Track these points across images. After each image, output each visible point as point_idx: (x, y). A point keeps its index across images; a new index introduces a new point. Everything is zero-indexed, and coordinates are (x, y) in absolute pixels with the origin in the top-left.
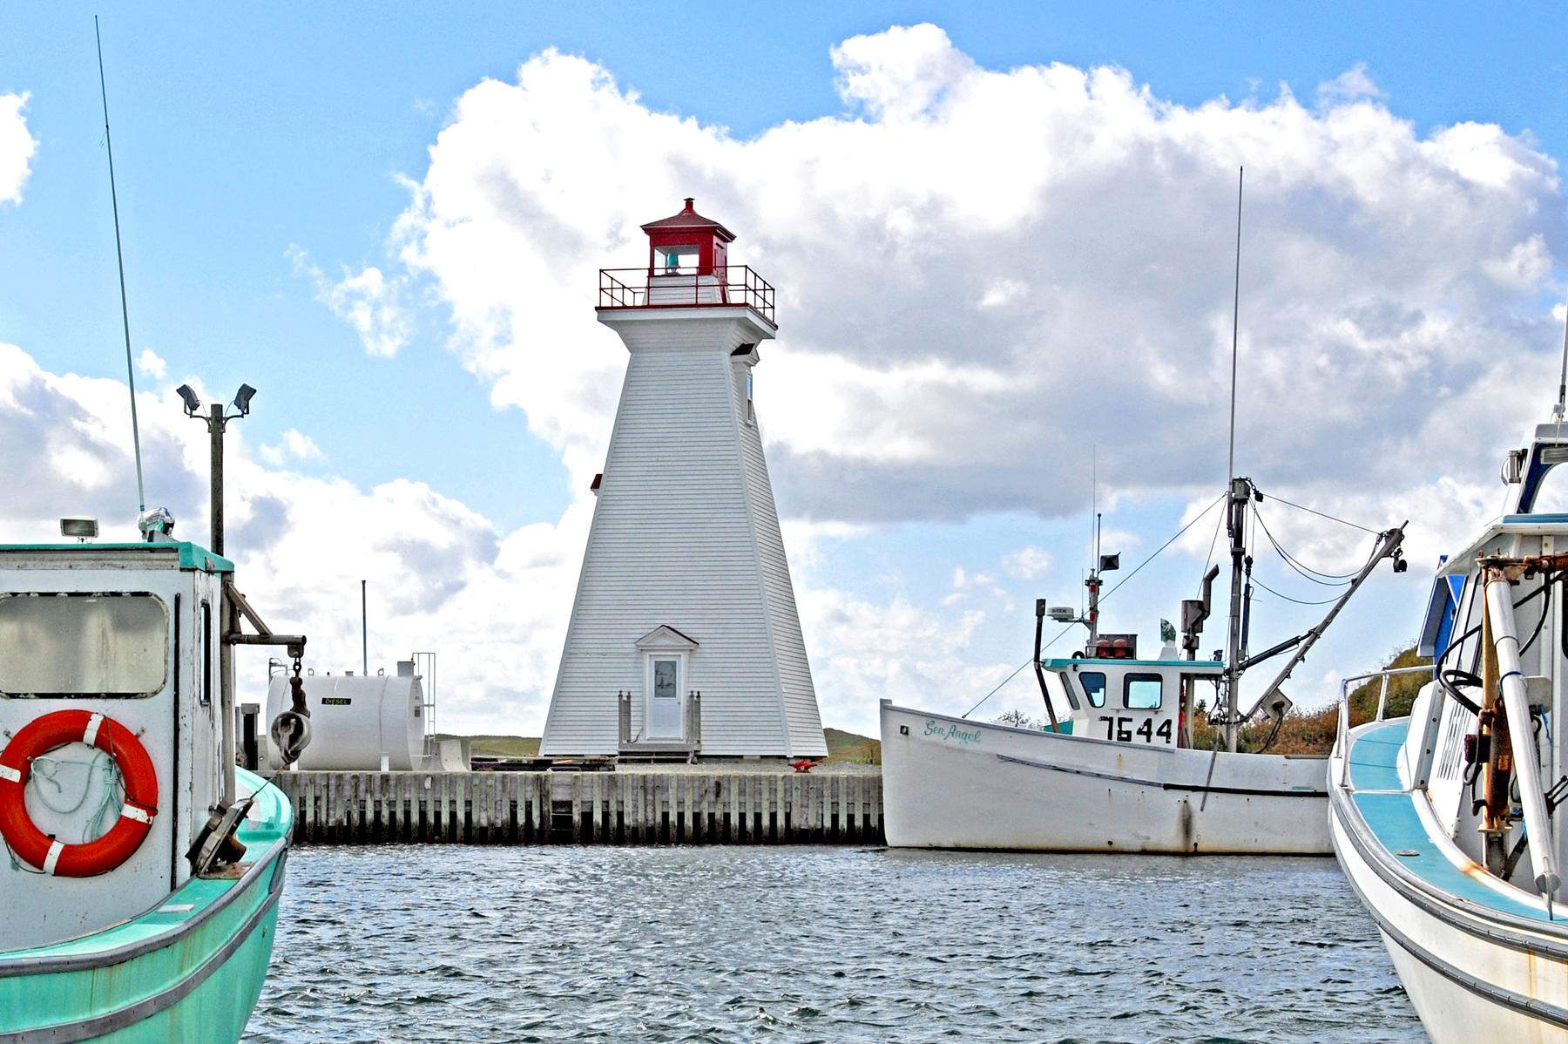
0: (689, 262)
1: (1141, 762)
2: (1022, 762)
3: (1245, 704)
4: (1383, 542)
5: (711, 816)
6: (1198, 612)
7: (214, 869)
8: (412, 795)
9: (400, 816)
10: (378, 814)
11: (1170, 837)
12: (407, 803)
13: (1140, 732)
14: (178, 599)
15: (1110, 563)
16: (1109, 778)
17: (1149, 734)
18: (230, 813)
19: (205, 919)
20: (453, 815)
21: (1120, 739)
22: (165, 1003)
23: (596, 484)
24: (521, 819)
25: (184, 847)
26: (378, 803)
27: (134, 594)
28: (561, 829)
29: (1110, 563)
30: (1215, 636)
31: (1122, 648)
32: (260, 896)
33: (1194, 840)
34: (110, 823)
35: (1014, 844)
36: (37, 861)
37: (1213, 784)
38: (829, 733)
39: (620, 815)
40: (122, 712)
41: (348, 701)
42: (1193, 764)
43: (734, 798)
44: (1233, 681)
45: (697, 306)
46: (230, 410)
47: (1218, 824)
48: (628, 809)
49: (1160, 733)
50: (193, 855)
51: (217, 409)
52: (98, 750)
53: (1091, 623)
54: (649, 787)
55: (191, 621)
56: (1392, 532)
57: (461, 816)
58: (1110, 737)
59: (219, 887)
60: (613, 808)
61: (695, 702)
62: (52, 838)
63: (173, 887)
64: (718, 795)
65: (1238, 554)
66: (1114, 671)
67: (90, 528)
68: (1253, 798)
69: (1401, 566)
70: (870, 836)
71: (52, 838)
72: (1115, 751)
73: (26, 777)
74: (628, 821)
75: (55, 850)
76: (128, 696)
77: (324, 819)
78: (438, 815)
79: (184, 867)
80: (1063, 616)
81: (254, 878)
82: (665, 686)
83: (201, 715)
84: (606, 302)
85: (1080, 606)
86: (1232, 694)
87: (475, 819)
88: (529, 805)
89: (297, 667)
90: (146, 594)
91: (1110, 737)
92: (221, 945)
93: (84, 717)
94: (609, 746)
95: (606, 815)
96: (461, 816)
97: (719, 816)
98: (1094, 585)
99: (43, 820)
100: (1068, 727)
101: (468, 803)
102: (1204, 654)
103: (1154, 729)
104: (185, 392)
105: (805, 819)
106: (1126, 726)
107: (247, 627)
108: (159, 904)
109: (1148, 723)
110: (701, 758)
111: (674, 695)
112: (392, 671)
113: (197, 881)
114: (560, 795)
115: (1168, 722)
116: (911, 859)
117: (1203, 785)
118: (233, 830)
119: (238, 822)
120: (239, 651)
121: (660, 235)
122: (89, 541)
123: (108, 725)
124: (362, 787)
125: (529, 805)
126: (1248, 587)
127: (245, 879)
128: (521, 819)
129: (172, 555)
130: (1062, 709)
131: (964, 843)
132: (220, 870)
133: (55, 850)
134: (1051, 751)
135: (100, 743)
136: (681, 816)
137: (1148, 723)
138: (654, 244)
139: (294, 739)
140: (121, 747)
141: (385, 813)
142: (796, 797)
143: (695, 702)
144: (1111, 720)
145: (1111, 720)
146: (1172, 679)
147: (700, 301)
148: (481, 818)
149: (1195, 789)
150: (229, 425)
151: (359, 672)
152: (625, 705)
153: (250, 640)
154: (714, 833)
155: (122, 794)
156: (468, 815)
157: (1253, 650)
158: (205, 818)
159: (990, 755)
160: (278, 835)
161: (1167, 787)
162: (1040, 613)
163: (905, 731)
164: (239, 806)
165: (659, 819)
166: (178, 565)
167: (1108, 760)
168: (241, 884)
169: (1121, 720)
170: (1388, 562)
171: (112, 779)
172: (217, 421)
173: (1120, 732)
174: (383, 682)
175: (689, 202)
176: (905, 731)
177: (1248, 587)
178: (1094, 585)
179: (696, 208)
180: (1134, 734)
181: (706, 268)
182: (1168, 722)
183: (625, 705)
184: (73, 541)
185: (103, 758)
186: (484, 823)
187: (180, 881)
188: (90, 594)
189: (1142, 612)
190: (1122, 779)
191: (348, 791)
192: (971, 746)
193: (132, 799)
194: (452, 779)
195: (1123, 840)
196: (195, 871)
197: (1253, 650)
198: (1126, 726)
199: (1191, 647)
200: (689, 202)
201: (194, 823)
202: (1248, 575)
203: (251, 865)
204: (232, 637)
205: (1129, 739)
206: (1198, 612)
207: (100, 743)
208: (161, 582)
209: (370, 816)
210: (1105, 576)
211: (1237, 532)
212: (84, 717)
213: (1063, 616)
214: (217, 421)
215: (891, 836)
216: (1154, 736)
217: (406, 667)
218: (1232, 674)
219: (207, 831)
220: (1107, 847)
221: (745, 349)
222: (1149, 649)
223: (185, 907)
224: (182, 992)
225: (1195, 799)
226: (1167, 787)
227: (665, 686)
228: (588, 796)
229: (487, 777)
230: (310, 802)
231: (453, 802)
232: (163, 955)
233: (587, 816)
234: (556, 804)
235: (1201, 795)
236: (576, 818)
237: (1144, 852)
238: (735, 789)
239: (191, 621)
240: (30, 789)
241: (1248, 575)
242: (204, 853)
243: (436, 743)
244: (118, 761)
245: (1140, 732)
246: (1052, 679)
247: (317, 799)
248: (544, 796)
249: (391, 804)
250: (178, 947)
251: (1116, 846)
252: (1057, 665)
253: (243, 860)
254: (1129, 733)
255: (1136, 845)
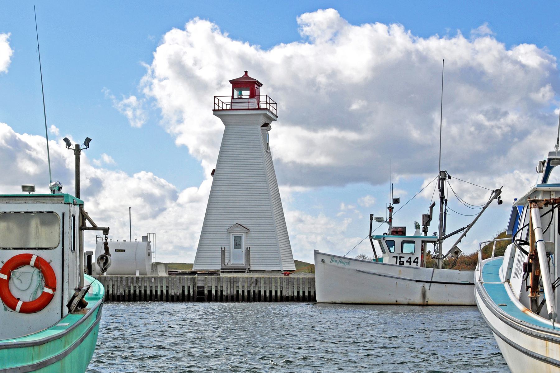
0: (246, 94)
1: (407, 272)
2: (365, 272)
3: (445, 252)
4: (494, 194)
5: (254, 291)
6: (428, 219)
7: (76, 310)
8: (147, 284)
9: (143, 292)
10: (135, 291)
11: (418, 299)
12: (145, 287)
13: (407, 262)
14: (63, 214)
15: (396, 201)
16: (396, 278)
17: (410, 262)
18: (82, 291)
19: (73, 328)
20: (162, 291)
21: (400, 264)
22: (59, 358)
23: (213, 173)
24: (186, 293)
25: (66, 303)
26: (135, 287)
27: (48, 212)
28: (201, 296)
29: (396, 201)
30: (434, 227)
31: (400, 232)
32: (93, 320)
33: (426, 300)
34: (39, 294)
35: (362, 301)
36: (14, 308)
37: (433, 280)
38: (296, 262)
39: (222, 291)
40: (44, 255)
41: (124, 251)
42: (426, 273)
43: (262, 285)
44: (440, 244)
45: (249, 109)
46: (82, 146)
47: (435, 294)
48: (224, 289)
49: (414, 262)
50: (69, 306)
51: (77, 146)
52: (35, 268)
53: (390, 223)
54: (232, 281)
55: (68, 222)
56: (497, 190)
57: (165, 292)
58: (396, 263)
59: (78, 317)
60: (219, 289)
61: (248, 251)
62: (19, 299)
63: (62, 317)
64: (256, 284)
65: (442, 198)
66: (398, 240)
67: (32, 189)
68: (447, 285)
69: (500, 202)
70: (311, 299)
71: (19, 299)
72: (398, 268)
73: (9, 278)
74: (224, 293)
75: (20, 304)
76: (46, 249)
77: (116, 293)
78: (156, 291)
79: (66, 310)
80: (380, 220)
81: (91, 314)
82: (237, 245)
83: (72, 255)
84: (217, 108)
85: (386, 217)
86: (440, 248)
87: (169, 292)
88: (189, 288)
89: (106, 238)
90: (52, 212)
91: (396, 263)
92: (79, 338)
93: (30, 256)
94: (217, 267)
95: (216, 291)
96: (165, 292)
97: (257, 291)
98: (391, 209)
99: (15, 293)
100: (381, 260)
101: (167, 287)
102: (430, 234)
103: (412, 260)
104: (66, 140)
105: (287, 293)
106: (402, 260)
107: (88, 224)
108: (57, 323)
109: (410, 258)
110: (250, 271)
111: (241, 248)
112: (140, 240)
113: (70, 315)
114: (200, 284)
115: (417, 258)
116: (325, 307)
117: (430, 280)
118: (83, 296)
119: (85, 294)
120: (85, 232)
121: (236, 84)
122: (32, 193)
123: (38, 259)
124: (129, 281)
125: (189, 288)
126: (446, 210)
127: (88, 314)
128: (186, 293)
129: (62, 198)
130: (379, 253)
131: (344, 301)
132: (78, 311)
133: (20, 304)
134: (375, 269)
135: (36, 265)
136: (243, 292)
137: (410, 258)
138: (234, 88)
139: (105, 264)
140: (43, 267)
141: (138, 290)
142: (284, 285)
143: (248, 251)
144: (397, 257)
145: (397, 257)
146: (419, 242)
147: (250, 108)
148: (172, 292)
149: (427, 282)
150: (82, 152)
151: (128, 240)
152: (223, 252)
153: (89, 229)
154: (255, 298)
155: (44, 284)
156: (167, 291)
157: (447, 232)
158: (73, 292)
159: (354, 270)
160: (99, 299)
161: (417, 281)
162: (372, 219)
163: (323, 261)
164: (85, 288)
165: (235, 292)
166: (63, 202)
167: (395, 272)
168: (86, 316)
169: (400, 257)
170: (496, 201)
171: (40, 278)
172: (77, 151)
173: (400, 262)
174: (137, 243)
175: (246, 72)
176: (323, 261)
177: (446, 210)
178: (391, 209)
179: (249, 74)
180: (405, 262)
181: (252, 96)
182: (417, 258)
183: (223, 252)
184: (26, 193)
185: (36, 271)
186: (173, 294)
187: (64, 315)
188: (32, 212)
189: (408, 219)
190: (401, 278)
191: (124, 283)
192: (347, 267)
193: (47, 286)
194: (161, 278)
195: (401, 300)
196: (70, 311)
197: (447, 232)
198: (402, 260)
199: (425, 231)
200: (246, 72)
201: (69, 294)
202: (446, 205)
203: (90, 309)
204: (83, 227)
205: (403, 264)
206: (428, 219)
207: (36, 265)
208: (58, 208)
209: (132, 291)
210: (395, 206)
211: (442, 190)
212: (30, 256)
213: (380, 220)
214: (77, 151)
215: (318, 299)
216: (412, 263)
217: (145, 238)
218: (440, 241)
219: (74, 297)
220: (395, 302)
221: (266, 125)
222: (410, 232)
223: (66, 324)
224: (65, 354)
225: (427, 285)
226: (417, 281)
227: (237, 245)
228: (210, 285)
229: (174, 278)
230: (111, 287)
231: (162, 287)
232: (58, 341)
233: (210, 292)
234: (198, 287)
235: (429, 284)
236: (206, 292)
237: (409, 305)
238: (262, 282)
239: (68, 222)
240: (11, 282)
241: (446, 205)
242: (73, 305)
243: (156, 266)
244: (42, 272)
245: (407, 262)
246: (376, 243)
247: (113, 285)
248: (194, 284)
249: (140, 287)
250: (64, 338)
251: (398, 302)
252: (377, 238)
253: (87, 307)
254: (403, 262)
255: (406, 302)
